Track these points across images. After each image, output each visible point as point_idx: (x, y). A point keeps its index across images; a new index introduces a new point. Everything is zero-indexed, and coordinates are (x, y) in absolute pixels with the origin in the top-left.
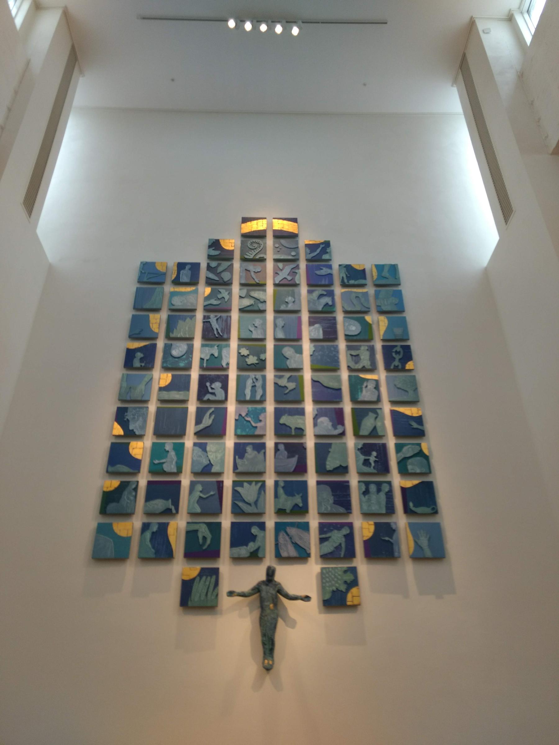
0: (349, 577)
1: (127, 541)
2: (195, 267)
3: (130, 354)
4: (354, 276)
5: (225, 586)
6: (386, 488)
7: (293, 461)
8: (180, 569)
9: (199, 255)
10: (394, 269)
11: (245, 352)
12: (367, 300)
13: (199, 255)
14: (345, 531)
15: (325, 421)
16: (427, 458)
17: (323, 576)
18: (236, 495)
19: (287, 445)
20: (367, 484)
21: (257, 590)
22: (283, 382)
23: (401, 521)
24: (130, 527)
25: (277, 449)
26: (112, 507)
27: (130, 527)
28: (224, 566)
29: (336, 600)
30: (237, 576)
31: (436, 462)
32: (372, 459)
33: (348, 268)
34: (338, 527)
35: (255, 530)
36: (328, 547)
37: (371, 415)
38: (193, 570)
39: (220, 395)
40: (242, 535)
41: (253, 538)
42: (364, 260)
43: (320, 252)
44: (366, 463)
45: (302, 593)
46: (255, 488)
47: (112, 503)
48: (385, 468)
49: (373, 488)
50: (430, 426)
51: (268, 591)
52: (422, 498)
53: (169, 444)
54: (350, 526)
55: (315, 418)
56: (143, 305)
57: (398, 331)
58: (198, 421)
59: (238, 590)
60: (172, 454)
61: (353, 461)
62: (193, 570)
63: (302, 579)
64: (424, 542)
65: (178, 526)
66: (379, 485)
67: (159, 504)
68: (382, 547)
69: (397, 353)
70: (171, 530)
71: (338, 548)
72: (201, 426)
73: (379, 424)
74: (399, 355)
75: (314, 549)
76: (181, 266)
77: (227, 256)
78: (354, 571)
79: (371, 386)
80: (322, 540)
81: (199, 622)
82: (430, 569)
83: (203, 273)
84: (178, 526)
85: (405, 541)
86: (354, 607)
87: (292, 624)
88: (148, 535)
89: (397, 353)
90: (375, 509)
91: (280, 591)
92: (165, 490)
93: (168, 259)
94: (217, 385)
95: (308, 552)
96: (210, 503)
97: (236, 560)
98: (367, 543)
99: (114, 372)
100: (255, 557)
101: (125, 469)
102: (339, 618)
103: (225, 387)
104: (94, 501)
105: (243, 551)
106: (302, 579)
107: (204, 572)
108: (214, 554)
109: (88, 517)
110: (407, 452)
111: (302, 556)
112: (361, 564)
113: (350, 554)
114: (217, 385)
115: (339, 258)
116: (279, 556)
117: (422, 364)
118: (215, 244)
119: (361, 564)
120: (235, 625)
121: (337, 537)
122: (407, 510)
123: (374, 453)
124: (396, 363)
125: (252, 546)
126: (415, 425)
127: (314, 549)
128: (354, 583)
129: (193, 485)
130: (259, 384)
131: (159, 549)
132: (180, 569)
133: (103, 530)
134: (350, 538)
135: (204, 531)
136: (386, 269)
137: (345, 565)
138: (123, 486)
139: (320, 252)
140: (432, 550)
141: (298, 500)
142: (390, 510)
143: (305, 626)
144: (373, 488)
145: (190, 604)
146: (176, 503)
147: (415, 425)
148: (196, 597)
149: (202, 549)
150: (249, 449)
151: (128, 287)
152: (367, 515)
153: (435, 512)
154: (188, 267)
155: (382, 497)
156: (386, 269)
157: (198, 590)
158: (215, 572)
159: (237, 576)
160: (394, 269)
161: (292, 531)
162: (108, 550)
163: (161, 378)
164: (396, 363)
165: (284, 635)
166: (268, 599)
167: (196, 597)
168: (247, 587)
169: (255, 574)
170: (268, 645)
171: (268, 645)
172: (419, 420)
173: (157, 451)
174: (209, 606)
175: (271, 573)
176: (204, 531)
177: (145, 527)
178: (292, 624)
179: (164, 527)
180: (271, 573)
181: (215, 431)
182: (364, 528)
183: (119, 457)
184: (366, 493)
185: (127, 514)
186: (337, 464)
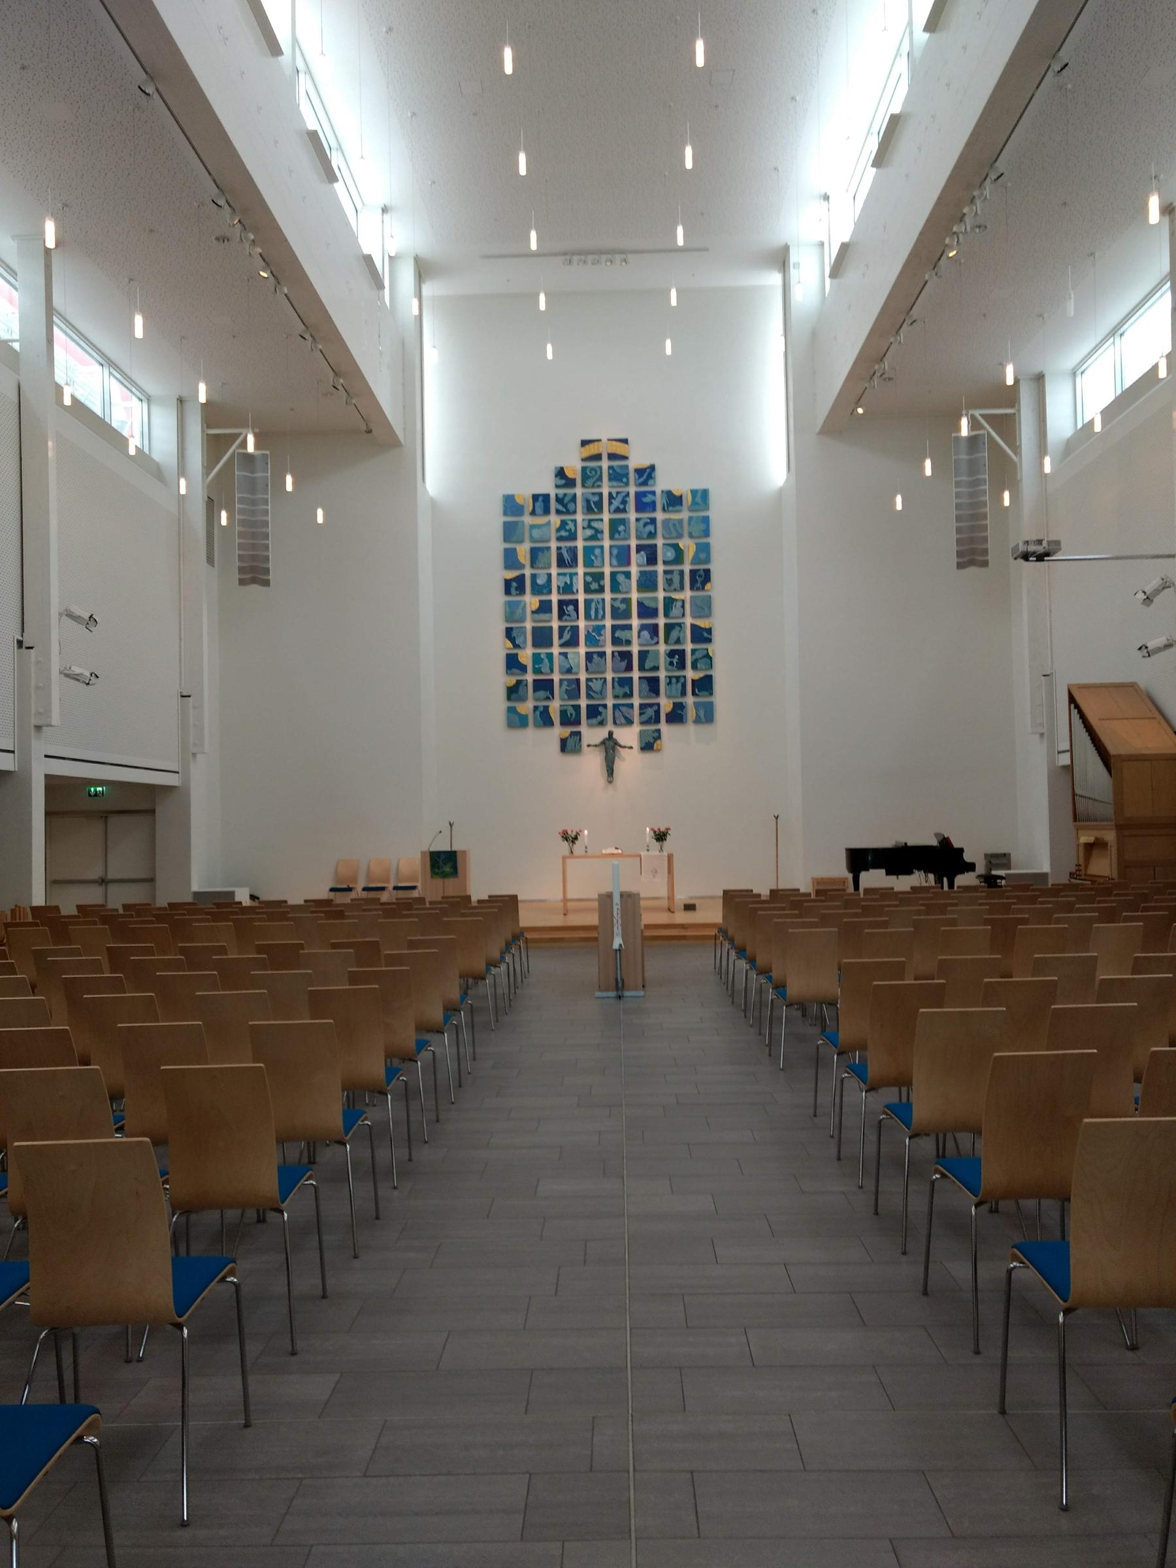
0: (656, 735)
1: (526, 716)
2: (546, 497)
3: (508, 583)
4: (673, 500)
5: (585, 742)
6: (682, 680)
7: (624, 664)
8: (558, 731)
9: (548, 486)
10: (705, 493)
11: (589, 579)
12: (682, 527)
13: (548, 486)
14: (655, 708)
15: (645, 633)
16: (711, 658)
17: (641, 733)
18: (588, 688)
19: (619, 652)
20: (670, 678)
21: (603, 743)
22: (617, 604)
23: (690, 700)
24: (526, 707)
25: (613, 655)
26: (514, 696)
27: (526, 707)
28: (583, 729)
29: (648, 745)
30: (592, 735)
31: (717, 662)
32: (675, 661)
33: (669, 494)
34: (651, 705)
35: (601, 709)
36: (645, 717)
37: (678, 628)
38: (567, 731)
39: (573, 614)
40: (593, 712)
41: (600, 713)
42: (681, 487)
43: (647, 474)
44: (671, 663)
45: (628, 745)
46: (600, 683)
47: (513, 692)
48: (682, 666)
49: (674, 680)
50: (717, 636)
51: (611, 743)
52: (705, 685)
53: (543, 651)
54: (658, 705)
55: (639, 633)
56: (510, 532)
57: (702, 556)
58: (560, 637)
59: (592, 743)
60: (546, 661)
61: (662, 661)
62: (567, 731)
63: (629, 736)
64: (702, 714)
65: (555, 706)
66: (678, 678)
67: (542, 694)
68: (676, 716)
69: (700, 576)
70: (550, 710)
71: (651, 718)
72: (563, 640)
73: (682, 635)
74: (701, 578)
75: (636, 719)
76: (535, 497)
77: (571, 483)
78: (659, 731)
79: (679, 604)
80: (641, 714)
81: (571, 760)
82: (705, 729)
83: (553, 504)
84: (555, 706)
85: (691, 713)
86: (658, 750)
87: (623, 760)
88: (538, 713)
89: (700, 576)
90: (674, 693)
91: (616, 743)
92: (544, 686)
93: (524, 492)
94: (571, 608)
95: (1167, 219)
96: (573, 689)
97: (590, 726)
98: (667, 715)
99: (499, 599)
100: (602, 723)
101: (517, 671)
102: (649, 756)
103: (577, 610)
104: (502, 694)
105: (594, 721)
106: (629, 736)
107: (572, 734)
108: (578, 723)
109: (500, 703)
110: (698, 655)
111: (630, 722)
112: (664, 727)
113: (657, 721)
114: (571, 608)
115: (662, 483)
116: (615, 723)
117: (717, 588)
118: (560, 473)
119: (664, 727)
120: (591, 762)
121: (650, 712)
122: (694, 694)
123: (677, 658)
124: (699, 585)
125: (599, 718)
126: (706, 635)
127: (636, 719)
128: (659, 737)
129: (561, 681)
130: (600, 606)
131: (545, 720)
132: (558, 731)
133: (511, 711)
134: (658, 713)
135: (571, 710)
136: (699, 494)
137: (653, 727)
138: (519, 682)
139: (647, 474)
140: (707, 716)
141: (627, 690)
142: (684, 693)
143: (631, 761)
144: (674, 680)
145: (671, 615)
146: (552, 694)
147: (706, 635)
148: (570, 746)
149: (570, 719)
150: (595, 656)
151: (496, 520)
152: (669, 697)
153: (711, 694)
154: (541, 499)
155: (680, 685)
156: (699, 494)
157: (570, 743)
158: (579, 733)
159: (592, 735)
160: (705, 493)
161: (623, 709)
162: (516, 721)
163: (531, 601)
164: (699, 585)
165: (619, 766)
166: (610, 746)
167: (570, 746)
168: (598, 741)
169: (601, 734)
170: (610, 771)
171: (610, 771)
172: (709, 631)
173: (536, 658)
174: (577, 750)
175: (611, 734)
176: (571, 710)
177: (536, 708)
178: (623, 760)
179: (546, 708)
180: (611, 734)
181: (573, 642)
182: (666, 704)
183: (513, 663)
184: (669, 683)
185: (523, 699)
186: (652, 665)
